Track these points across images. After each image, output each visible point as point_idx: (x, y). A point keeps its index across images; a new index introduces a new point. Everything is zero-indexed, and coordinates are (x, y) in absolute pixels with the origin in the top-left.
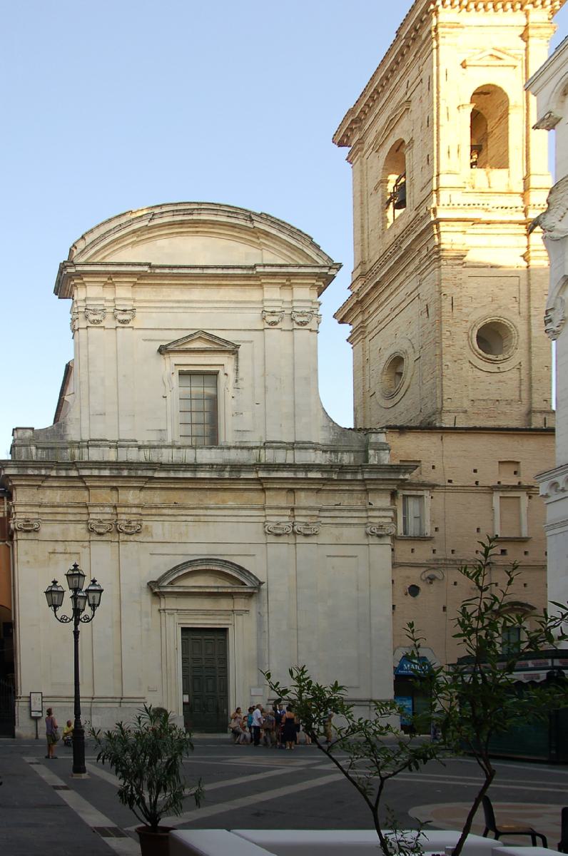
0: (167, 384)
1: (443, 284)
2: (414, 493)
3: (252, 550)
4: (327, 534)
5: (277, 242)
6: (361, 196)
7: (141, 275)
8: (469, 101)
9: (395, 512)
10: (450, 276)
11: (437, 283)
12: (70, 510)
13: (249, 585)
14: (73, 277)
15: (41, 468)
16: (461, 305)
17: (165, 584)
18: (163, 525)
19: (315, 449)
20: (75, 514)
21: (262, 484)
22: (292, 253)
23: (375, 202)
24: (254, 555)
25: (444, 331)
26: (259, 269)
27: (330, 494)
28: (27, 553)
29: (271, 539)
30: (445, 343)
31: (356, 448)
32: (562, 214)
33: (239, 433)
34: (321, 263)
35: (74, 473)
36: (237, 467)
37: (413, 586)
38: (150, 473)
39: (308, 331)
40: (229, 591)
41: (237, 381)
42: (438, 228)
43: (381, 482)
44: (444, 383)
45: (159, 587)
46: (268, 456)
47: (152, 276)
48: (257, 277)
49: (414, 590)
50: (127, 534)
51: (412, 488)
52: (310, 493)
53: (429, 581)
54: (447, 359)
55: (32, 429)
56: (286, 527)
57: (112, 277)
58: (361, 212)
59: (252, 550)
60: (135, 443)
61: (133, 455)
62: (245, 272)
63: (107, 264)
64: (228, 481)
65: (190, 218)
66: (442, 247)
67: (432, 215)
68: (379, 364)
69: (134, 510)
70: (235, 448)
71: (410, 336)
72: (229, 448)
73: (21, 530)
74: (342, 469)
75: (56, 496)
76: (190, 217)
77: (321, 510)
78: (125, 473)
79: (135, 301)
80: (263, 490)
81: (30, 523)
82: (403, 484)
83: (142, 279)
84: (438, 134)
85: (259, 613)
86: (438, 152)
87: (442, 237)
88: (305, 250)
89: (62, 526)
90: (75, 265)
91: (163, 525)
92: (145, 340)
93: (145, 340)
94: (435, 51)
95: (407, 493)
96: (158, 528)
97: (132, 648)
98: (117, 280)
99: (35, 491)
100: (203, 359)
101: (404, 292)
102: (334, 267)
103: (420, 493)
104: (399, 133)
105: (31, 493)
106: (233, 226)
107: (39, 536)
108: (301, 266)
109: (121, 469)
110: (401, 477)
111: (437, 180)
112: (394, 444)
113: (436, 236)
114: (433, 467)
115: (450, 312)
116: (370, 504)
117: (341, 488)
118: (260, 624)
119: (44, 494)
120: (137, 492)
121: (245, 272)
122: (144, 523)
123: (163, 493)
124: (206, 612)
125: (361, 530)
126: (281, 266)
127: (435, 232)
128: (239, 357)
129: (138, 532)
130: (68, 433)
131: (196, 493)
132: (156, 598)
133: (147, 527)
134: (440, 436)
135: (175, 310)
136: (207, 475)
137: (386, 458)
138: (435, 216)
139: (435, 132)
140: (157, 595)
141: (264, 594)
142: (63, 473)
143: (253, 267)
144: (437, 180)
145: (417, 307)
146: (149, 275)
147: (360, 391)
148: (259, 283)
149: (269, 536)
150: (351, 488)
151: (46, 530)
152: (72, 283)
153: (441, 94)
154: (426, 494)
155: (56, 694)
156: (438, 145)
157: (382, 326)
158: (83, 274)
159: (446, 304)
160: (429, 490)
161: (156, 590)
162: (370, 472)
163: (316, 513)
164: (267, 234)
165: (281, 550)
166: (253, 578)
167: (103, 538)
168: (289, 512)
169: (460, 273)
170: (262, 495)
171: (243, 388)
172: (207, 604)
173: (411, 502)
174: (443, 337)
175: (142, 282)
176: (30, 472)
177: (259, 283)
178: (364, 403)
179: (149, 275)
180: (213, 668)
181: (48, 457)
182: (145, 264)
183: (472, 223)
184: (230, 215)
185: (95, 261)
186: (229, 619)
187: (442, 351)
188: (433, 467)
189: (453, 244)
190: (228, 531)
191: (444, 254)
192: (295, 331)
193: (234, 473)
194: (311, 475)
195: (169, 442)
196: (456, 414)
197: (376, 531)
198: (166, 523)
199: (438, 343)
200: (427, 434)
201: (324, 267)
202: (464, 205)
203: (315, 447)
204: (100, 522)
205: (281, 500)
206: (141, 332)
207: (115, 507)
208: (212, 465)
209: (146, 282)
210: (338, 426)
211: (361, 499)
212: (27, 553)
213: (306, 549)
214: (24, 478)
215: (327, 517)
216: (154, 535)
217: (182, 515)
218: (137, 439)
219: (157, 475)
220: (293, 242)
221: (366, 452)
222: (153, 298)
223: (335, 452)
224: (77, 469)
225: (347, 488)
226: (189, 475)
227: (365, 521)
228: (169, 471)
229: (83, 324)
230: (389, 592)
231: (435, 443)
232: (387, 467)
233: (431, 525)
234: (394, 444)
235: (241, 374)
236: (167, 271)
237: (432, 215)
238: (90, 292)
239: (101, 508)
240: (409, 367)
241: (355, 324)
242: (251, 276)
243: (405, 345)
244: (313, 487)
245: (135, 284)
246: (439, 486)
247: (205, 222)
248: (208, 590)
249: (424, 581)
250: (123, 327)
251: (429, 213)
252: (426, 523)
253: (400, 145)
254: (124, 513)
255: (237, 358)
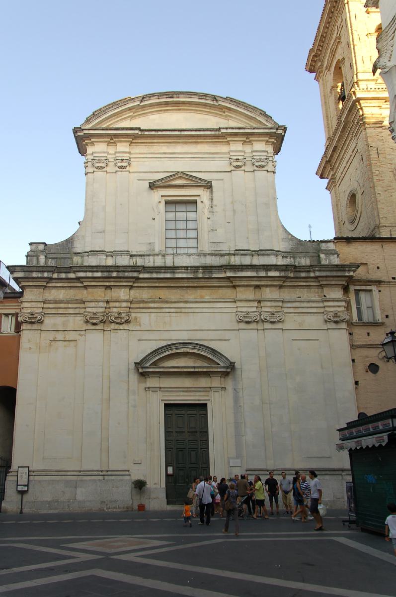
0: (156, 210)
1: (368, 140)
2: (364, 288)
3: (227, 335)
4: (291, 321)
5: (238, 114)
6: (325, 98)
7: (135, 137)
8: (374, 31)
9: (348, 303)
10: (374, 134)
11: (365, 139)
12: (70, 306)
13: (222, 364)
14: (84, 139)
15: (44, 272)
16: (385, 153)
17: (148, 365)
18: (150, 316)
19: (276, 255)
20: (76, 308)
21: (232, 282)
22: (250, 121)
23: (332, 100)
24: (229, 340)
25: (374, 171)
26: (223, 131)
27: (292, 290)
28: (29, 341)
29: (243, 326)
30: (375, 178)
31: (311, 254)
32: (389, 55)
33: (215, 245)
34: (270, 125)
35: (72, 276)
36: (208, 269)
37: (372, 364)
38: (135, 275)
39: (266, 172)
40: (205, 370)
41: (212, 207)
42: (360, 105)
43: (332, 279)
44: (378, 206)
45: (142, 368)
46: (236, 260)
47: (143, 137)
48: (223, 136)
49: (373, 368)
50: (117, 323)
51: (360, 284)
52: (274, 289)
53: (386, 360)
54: (378, 189)
55: (45, 244)
56: (254, 316)
57: (113, 137)
58: (326, 107)
59: (227, 335)
60: (127, 252)
61: (124, 261)
62: (213, 133)
63: (111, 129)
64: (203, 280)
65: (171, 100)
66: (365, 116)
67: (353, 96)
68: (344, 199)
69: (124, 304)
70: (211, 255)
71: (357, 179)
72: (205, 255)
73: (26, 322)
74: (295, 268)
75: (61, 294)
76: (172, 100)
77: (283, 302)
78: (114, 274)
79: (131, 154)
80: (234, 287)
81: (35, 316)
82: (351, 280)
83: (136, 139)
84: (354, 50)
85: (235, 389)
86: (356, 61)
87: (364, 110)
88: (257, 118)
89: (63, 319)
90: (83, 130)
91: (150, 316)
92: (139, 180)
93: (139, 180)
94: (346, 5)
95: (358, 288)
96: (146, 319)
97: (119, 424)
98: (117, 140)
99: (41, 290)
100: (184, 192)
101: (351, 151)
102: (280, 128)
103: (368, 288)
104: (338, 57)
105: (38, 292)
106: (205, 105)
107: (43, 327)
108: (254, 128)
109: (110, 271)
110: (347, 274)
111: (357, 76)
112: (343, 251)
113: (360, 110)
114: (378, 268)
115: (376, 158)
116: (325, 296)
117: (300, 284)
118: (236, 399)
119: (50, 293)
120: (127, 290)
121: (213, 133)
122: (133, 315)
123: (151, 290)
124: (187, 389)
125: (321, 318)
126: (239, 128)
127: (359, 107)
128: (214, 190)
129: (127, 322)
130: (75, 246)
131: (179, 291)
132: (143, 378)
133: (136, 318)
134: (380, 244)
135: (162, 159)
136: (184, 276)
137: (335, 260)
138: (355, 97)
139: (352, 49)
140: (143, 375)
141: (238, 372)
142: (63, 276)
143: (219, 129)
144: (357, 76)
145: (358, 157)
146: (138, 136)
147: (337, 223)
148: (226, 140)
149: (240, 324)
150: (308, 284)
151: (49, 322)
152: (84, 143)
153: (353, 28)
154: (374, 288)
155: (47, 468)
156: (355, 57)
157: (343, 175)
158: (91, 136)
159: (373, 153)
160: (377, 285)
161: (142, 370)
162: (320, 271)
163: (280, 304)
164: (229, 109)
165: (250, 335)
166: (225, 359)
167: (97, 327)
168: (256, 304)
169: (381, 132)
170: (234, 291)
171: (217, 212)
172: (187, 382)
173: (362, 296)
174: (374, 174)
175: (136, 141)
176: (34, 275)
177: (226, 140)
178: (340, 230)
179: (138, 136)
180: (196, 440)
181: (51, 266)
182: (136, 129)
183: (384, 101)
184: (200, 97)
185: (103, 127)
186: (208, 396)
187: (374, 184)
188: (378, 268)
189: (373, 114)
190: (206, 320)
191: (367, 120)
192: (255, 172)
193: (206, 274)
194: (270, 274)
195: (157, 251)
196: (391, 228)
197: (332, 318)
198: (153, 315)
199: (370, 179)
200: (370, 243)
201: (271, 128)
202: (375, 89)
203: (276, 254)
204: (95, 314)
205: (250, 294)
206: (136, 174)
207: (107, 302)
208: (187, 267)
209: (139, 141)
210: (296, 238)
211: (318, 293)
212: (29, 341)
213: (272, 335)
214: (30, 280)
215: (290, 308)
216: (142, 324)
217: (166, 308)
218: (129, 250)
219: (141, 276)
220: (249, 113)
221: (319, 256)
222: (145, 152)
223: (294, 257)
224: (74, 272)
225: (305, 284)
226: (168, 275)
227: (322, 310)
228: (152, 273)
229: (90, 170)
230: (349, 368)
231: (376, 250)
232: (333, 267)
233: (382, 313)
234: (343, 251)
235: (215, 202)
236: (153, 133)
237: (353, 96)
238: (97, 149)
239: (96, 303)
240: (359, 197)
241: (329, 178)
242: (218, 136)
243: (355, 185)
244: (275, 284)
245: (131, 143)
246: (385, 282)
247: (184, 103)
248: (185, 370)
249: (381, 359)
250: (121, 171)
251: (351, 95)
252: (377, 311)
253: (339, 62)
254: (116, 307)
255: (212, 191)
